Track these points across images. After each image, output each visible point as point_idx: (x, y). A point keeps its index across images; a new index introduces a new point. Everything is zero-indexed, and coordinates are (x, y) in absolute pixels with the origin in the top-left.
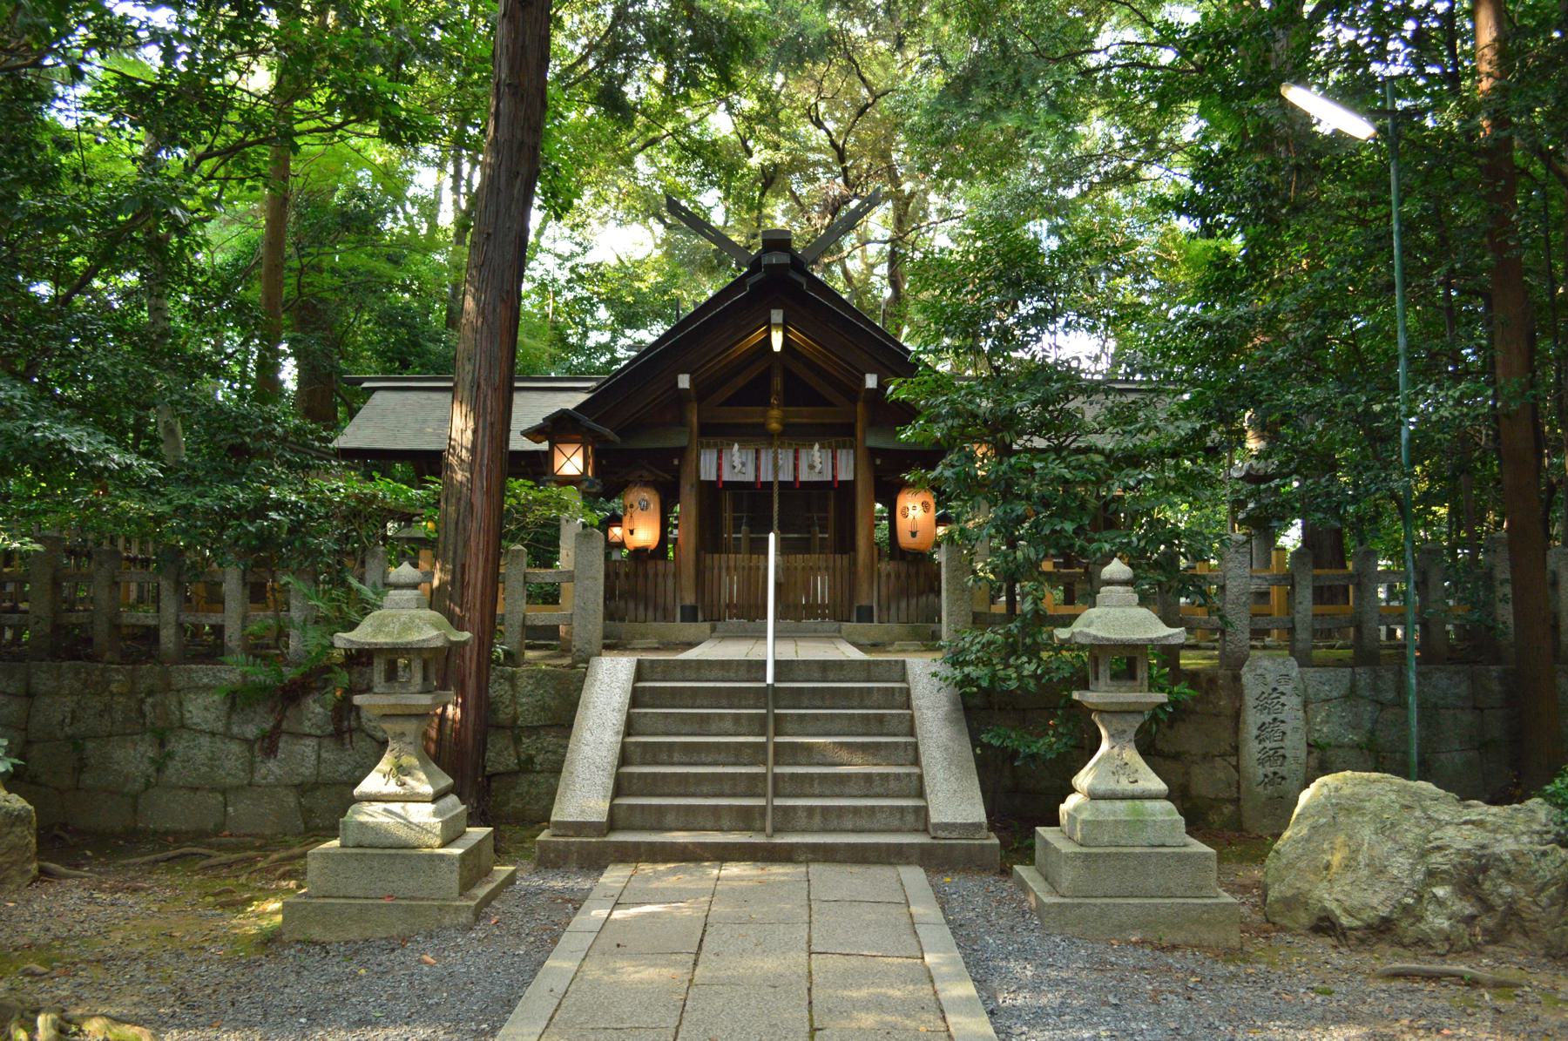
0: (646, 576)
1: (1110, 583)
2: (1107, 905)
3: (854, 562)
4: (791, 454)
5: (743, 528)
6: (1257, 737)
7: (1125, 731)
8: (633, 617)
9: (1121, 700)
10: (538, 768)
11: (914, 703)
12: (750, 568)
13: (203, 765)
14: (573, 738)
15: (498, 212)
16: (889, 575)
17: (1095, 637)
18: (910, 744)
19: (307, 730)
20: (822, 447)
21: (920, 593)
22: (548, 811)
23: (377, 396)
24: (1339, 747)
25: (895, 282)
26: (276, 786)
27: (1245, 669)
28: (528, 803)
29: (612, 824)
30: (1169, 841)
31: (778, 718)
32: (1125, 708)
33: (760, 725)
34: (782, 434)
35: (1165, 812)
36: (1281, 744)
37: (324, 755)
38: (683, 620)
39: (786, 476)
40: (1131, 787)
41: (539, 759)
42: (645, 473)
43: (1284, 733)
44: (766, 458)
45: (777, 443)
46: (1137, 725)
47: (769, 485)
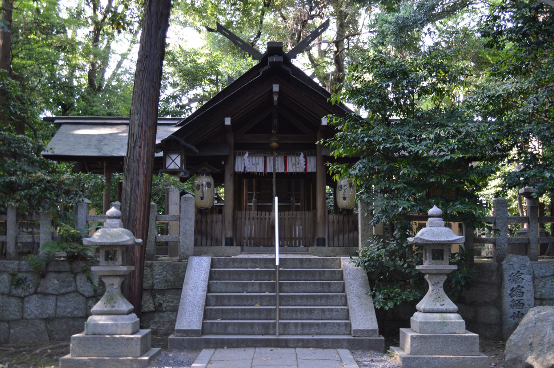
0: (207, 222)
1: (432, 216)
2: (430, 358)
3: (315, 215)
4: (283, 159)
5: (253, 200)
6: (510, 294)
7: (438, 283)
8: (200, 244)
9: (437, 268)
10: (164, 309)
11: (345, 277)
12: (261, 219)
14: (183, 293)
15: (151, 45)
16: (333, 222)
17: (424, 240)
18: (343, 296)
19: (51, 292)
21: (350, 231)
22: (173, 322)
23: (63, 127)
25: (338, 61)
26: (35, 319)
27: (504, 262)
28: (159, 327)
29: (203, 332)
31: (280, 284)
32: (438, 272)
33: (272, 287)
35: (455, 318)
36: (521, 298)
37: (59, 304)
38: (226, 245)
39: (281, 170)
40: (442, 307)
41: (165, 305)
42: (206, 169)
43: (523, 293)
44: (270, 160)
46: (444, 280)
47: (271, 174)
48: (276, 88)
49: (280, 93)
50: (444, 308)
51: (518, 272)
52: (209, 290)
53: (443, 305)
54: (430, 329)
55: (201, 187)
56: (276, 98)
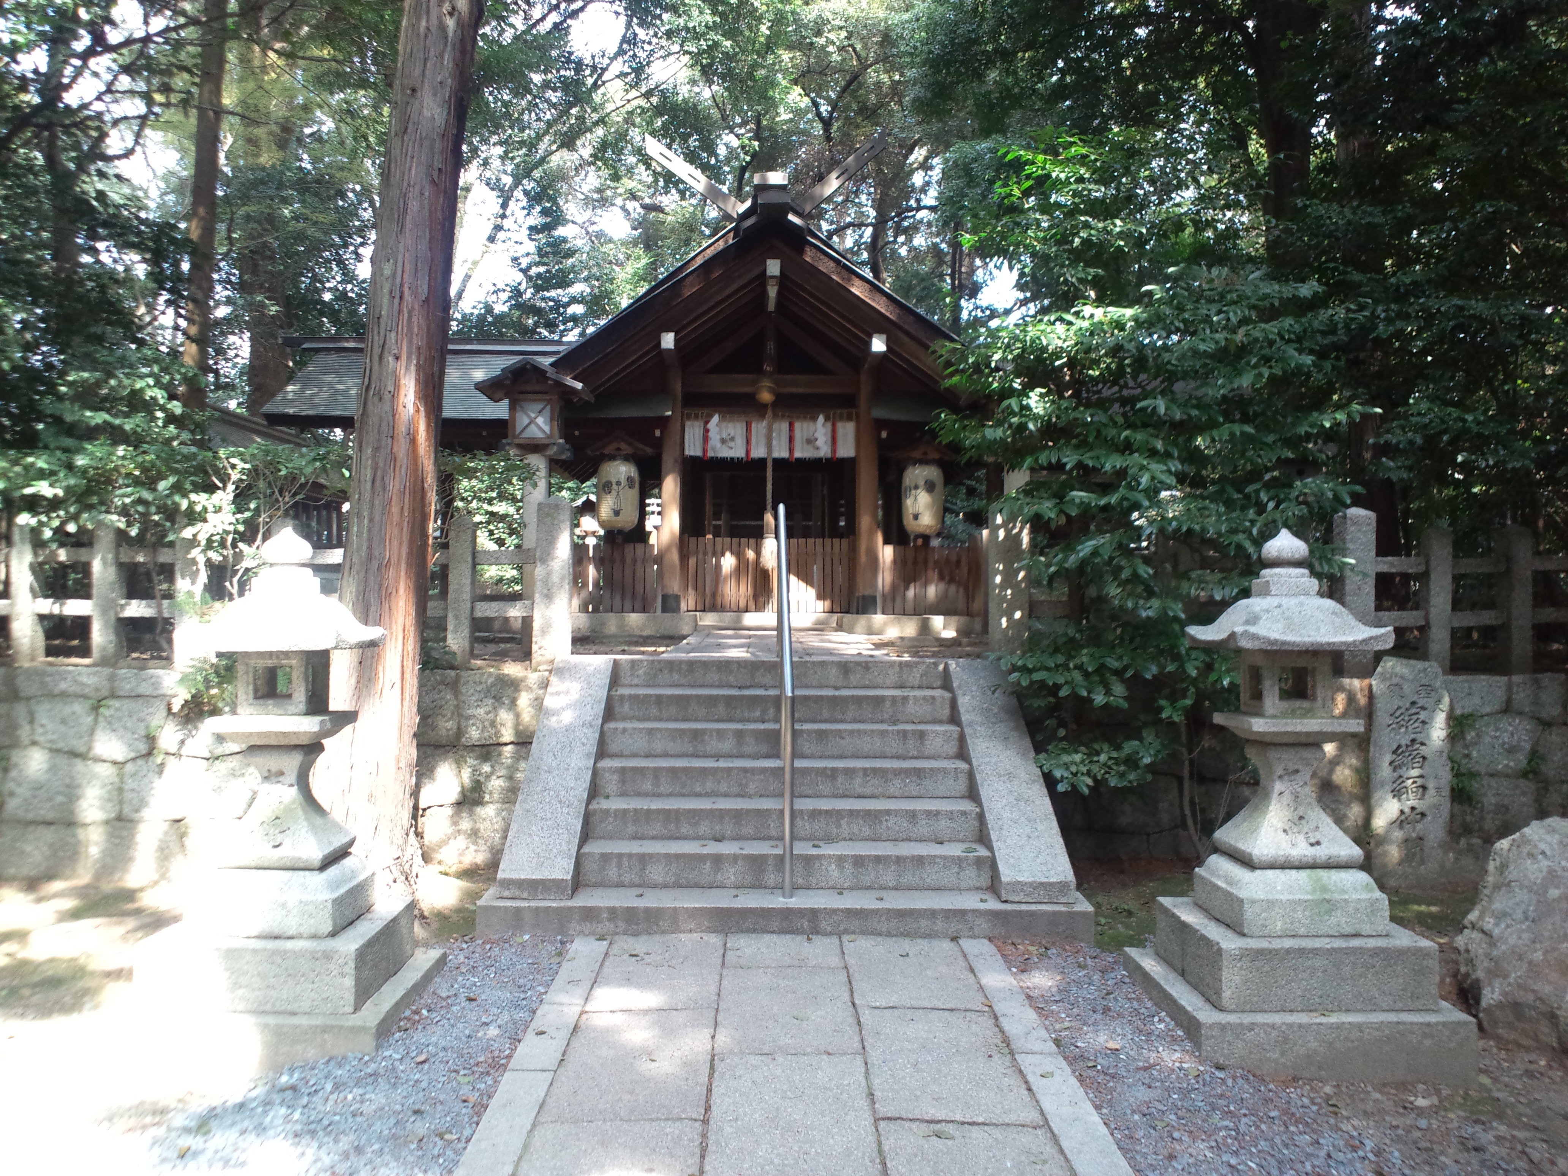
0: (623, 561)
7: (1297, 771)
13: (59, 793)
20: (827, 419)
24: (1492, 775)
30: (1366, 929)
32: (1303, 740)
34: (775, 404)
39: (780, 452)
42: (623, 446)
45: (769, 413)
47: (762, 462)
48: (773, 267)
49: (783, 279)
50: (1321, 853)
51: (1413, 703)
52: (602, 752)
53: (1318, 843)
54: (1279, 924)
55: (615, 487)
56: (772, 292)
